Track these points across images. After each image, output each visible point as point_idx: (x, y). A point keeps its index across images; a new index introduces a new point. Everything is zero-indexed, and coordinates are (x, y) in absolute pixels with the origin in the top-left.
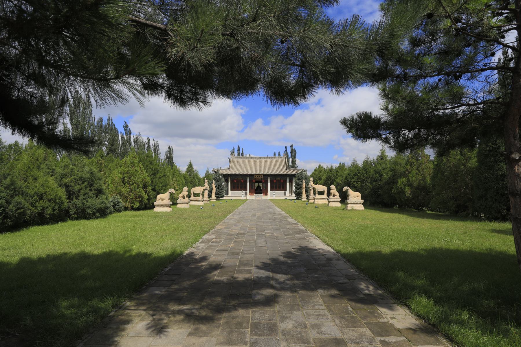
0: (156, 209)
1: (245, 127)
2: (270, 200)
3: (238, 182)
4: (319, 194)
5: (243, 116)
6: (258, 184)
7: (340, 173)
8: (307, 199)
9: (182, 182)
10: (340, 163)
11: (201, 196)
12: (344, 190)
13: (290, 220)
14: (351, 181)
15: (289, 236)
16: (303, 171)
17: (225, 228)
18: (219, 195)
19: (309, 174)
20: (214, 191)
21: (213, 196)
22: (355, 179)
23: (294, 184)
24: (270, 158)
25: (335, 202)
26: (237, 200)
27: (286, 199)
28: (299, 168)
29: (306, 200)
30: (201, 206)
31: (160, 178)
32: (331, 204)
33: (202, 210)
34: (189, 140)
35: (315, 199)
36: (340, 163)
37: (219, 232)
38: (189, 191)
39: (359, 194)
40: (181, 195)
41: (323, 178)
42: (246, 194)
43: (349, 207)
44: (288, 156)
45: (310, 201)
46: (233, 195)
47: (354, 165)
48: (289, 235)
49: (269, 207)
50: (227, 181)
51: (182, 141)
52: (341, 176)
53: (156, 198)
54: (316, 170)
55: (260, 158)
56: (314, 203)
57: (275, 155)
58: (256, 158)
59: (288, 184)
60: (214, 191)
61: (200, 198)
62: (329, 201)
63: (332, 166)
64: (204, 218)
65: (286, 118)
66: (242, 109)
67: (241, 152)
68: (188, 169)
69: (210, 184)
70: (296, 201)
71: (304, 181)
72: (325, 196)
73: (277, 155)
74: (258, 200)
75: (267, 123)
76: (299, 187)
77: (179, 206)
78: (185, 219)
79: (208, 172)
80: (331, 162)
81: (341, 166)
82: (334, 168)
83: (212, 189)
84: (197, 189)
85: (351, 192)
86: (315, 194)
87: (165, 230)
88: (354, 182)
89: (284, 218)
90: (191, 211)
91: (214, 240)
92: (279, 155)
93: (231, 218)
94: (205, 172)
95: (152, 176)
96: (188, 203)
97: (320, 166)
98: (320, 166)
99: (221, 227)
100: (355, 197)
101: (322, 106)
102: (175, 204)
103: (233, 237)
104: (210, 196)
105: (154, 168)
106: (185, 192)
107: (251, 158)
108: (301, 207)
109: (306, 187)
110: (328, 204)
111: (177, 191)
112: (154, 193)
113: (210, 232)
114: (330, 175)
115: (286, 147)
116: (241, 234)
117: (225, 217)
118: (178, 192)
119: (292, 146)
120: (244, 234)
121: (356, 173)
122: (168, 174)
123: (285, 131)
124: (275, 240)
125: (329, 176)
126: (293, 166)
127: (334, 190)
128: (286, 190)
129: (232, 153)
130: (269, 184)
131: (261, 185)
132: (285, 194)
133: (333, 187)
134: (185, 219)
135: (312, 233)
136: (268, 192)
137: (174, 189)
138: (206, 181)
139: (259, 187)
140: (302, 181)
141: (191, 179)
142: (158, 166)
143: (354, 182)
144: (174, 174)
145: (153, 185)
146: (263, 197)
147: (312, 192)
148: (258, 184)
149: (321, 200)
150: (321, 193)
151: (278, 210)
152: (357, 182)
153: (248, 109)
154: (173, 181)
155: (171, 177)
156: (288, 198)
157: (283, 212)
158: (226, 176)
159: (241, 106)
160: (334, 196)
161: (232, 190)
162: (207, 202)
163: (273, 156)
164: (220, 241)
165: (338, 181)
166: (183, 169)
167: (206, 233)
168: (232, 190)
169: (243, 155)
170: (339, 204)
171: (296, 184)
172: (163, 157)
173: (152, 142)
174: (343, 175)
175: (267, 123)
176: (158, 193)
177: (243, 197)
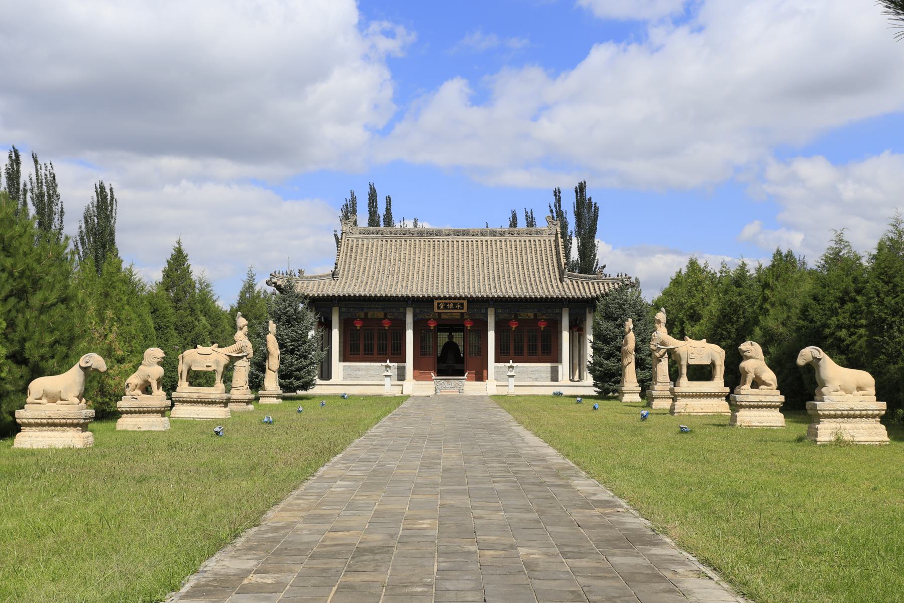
0: (25, 440)
1: (398, 117)
2: (496, 397)
3: (371, 325)
4: (691, 378)
5: (391, 62)
6: (450, 335)
7: (780, 291)
8: (642, 395)
9: (144, 328)
10: (779, 253)
11: (220, 386)
12: (801, 361)
13: (584, 485)
14: (825, 326)
15: (583, 563)
16: (628, 284)
17: (309, 519)
18: (294, 381)
19: (649, 296)
20: (274, 363)
21: (271, 382)
22: (843, 318)
23: (590, 337)
24: (493, 233)
25: (762, 410)
26: (367, 397)
27: (559, 394)
28: (611, 271)
29: (637, 398)
30: (216, 421)
31: (43, 309)
32: (745, 417)
33: (219, 441)
34: (172, 163)
35: (674, 397)
36: (779, 253)
37: (275, 541)
38: (169, 364)
39: (865, 378)
40: (134, 379)
41: (705, 312)
42: (401, 376)
43: (826, 431)
44: (564, 226)
45: (657, 404)
46: (349, 379)
47: (839, 261)
48: (581, 555)
49: (493, 428)
50: (325, 325)
51: (143, 166)
52: (783, 303)
53: (24, 391)
54: (677, 282)
55: (457, 233)
56: (672, 411)
57: (514, 223)
58: (439, 233)
59: (566, 335)
60: (274, 363)
61: (217, 391)
62: (735, 407)
63: (743, 266)
64: (221, 474)
65: (555, 76)
66: (389, 34)
67: (381, 211)
68: (167, 274)
69: (257, 336)
70: (598, 403)
71: (629, 324)
72: (718, 384)
73: (522, 224)
74: (451, 400)
75: (481, 97)
76: (610, 350)
77: (125, 423)
78: (142, 480)
79: (250, 287)
80: (739, 250)
81: (784, 263)
82: (752, 271)
83: (266, 356)
84: (205, 357)
85: (832, 371)
86: (674, 376)
87: (40, 535)
88: (839, 327)
89: (557, 476)
90: (171, 447)
91: (254, 579)
92: (531, 223)
93: (336, 476)
94: (239, 287)
95: (12, 301)
96: (162, 412)
97: (693, 265)
98: (693, 265)
99: (288, 517)
100: (848, 391)
101: (700, 29)
102: (106, 414)
103: (335, 564)
104: (256, 384)
105: (20, 267)
106: (151, 364)
107: (421, 233)
108: (621, 427)
109: (637, 350)
110: (733, 419)
111: (120, 361)
112: (20, 371)
113: (240, 541)
114: (736, 299)
115: (557, 193)
116: (371, 551)
117: (309, 469)
118: (126, 366)
119: (581, 189)
120: (385, 550)
121: (846, 292)
122: (80, 294)
123: (551, 129)
124: (523, 579)
125: (731, 304)
126: (587, 264)
127: (755, 360)
128: (556, 358)
129: (349, 211)
130: (491, 335)
131: (458, 338)
132: (555, 377)
133: (752, 348)
134: (142, 480)
135: (683, 545)
136: (485, 366)
137: (108, 354)
138: (242, 321)
139: (450, 346)
140: (622, 325)
141: (181, 312)
142: (39, 261)
143: (839, 327)
144: (107, 295)
145: (16, 337)
146: (470, 387)
147: (663, 368)
148: (450, 335)
149: (703, 402)
150: (702, 373)
151: (532, 442)
152: (852, 328)
153: (413, 37)
154: (102, 321)
155: (92, 308)
156: (566, 392)
157: (551, 451)
158: (322, 305)
159: (386, 25)
160: (756, 384)
161: (344, 358)
162: (243, 406)
163: (506, 226)
164: (277, 587)
165: (770, 323)
166: (149, 274)
167: (219, 545)
168: (344, 358)
169: (388, 221)
170: (776, 419)
171: (599, 336)
172: (72, 227)
173: (27, 171)
174: (790, 301)
175: (481, 97)
176: (38, 372)
177: (389, 388)
